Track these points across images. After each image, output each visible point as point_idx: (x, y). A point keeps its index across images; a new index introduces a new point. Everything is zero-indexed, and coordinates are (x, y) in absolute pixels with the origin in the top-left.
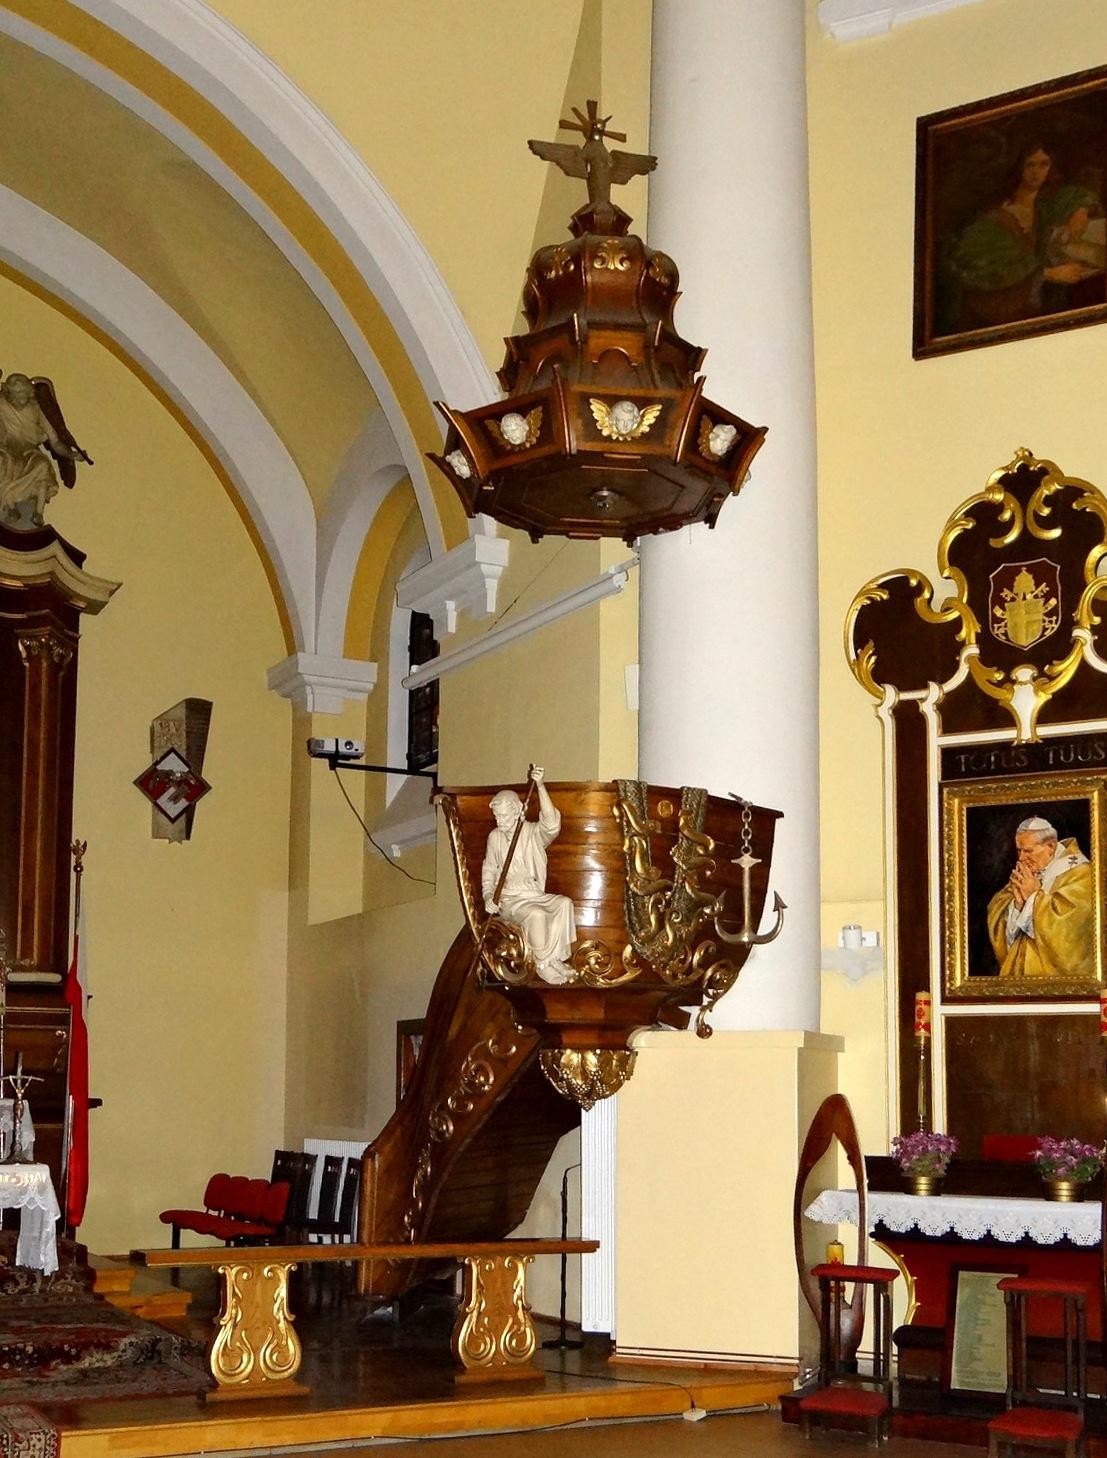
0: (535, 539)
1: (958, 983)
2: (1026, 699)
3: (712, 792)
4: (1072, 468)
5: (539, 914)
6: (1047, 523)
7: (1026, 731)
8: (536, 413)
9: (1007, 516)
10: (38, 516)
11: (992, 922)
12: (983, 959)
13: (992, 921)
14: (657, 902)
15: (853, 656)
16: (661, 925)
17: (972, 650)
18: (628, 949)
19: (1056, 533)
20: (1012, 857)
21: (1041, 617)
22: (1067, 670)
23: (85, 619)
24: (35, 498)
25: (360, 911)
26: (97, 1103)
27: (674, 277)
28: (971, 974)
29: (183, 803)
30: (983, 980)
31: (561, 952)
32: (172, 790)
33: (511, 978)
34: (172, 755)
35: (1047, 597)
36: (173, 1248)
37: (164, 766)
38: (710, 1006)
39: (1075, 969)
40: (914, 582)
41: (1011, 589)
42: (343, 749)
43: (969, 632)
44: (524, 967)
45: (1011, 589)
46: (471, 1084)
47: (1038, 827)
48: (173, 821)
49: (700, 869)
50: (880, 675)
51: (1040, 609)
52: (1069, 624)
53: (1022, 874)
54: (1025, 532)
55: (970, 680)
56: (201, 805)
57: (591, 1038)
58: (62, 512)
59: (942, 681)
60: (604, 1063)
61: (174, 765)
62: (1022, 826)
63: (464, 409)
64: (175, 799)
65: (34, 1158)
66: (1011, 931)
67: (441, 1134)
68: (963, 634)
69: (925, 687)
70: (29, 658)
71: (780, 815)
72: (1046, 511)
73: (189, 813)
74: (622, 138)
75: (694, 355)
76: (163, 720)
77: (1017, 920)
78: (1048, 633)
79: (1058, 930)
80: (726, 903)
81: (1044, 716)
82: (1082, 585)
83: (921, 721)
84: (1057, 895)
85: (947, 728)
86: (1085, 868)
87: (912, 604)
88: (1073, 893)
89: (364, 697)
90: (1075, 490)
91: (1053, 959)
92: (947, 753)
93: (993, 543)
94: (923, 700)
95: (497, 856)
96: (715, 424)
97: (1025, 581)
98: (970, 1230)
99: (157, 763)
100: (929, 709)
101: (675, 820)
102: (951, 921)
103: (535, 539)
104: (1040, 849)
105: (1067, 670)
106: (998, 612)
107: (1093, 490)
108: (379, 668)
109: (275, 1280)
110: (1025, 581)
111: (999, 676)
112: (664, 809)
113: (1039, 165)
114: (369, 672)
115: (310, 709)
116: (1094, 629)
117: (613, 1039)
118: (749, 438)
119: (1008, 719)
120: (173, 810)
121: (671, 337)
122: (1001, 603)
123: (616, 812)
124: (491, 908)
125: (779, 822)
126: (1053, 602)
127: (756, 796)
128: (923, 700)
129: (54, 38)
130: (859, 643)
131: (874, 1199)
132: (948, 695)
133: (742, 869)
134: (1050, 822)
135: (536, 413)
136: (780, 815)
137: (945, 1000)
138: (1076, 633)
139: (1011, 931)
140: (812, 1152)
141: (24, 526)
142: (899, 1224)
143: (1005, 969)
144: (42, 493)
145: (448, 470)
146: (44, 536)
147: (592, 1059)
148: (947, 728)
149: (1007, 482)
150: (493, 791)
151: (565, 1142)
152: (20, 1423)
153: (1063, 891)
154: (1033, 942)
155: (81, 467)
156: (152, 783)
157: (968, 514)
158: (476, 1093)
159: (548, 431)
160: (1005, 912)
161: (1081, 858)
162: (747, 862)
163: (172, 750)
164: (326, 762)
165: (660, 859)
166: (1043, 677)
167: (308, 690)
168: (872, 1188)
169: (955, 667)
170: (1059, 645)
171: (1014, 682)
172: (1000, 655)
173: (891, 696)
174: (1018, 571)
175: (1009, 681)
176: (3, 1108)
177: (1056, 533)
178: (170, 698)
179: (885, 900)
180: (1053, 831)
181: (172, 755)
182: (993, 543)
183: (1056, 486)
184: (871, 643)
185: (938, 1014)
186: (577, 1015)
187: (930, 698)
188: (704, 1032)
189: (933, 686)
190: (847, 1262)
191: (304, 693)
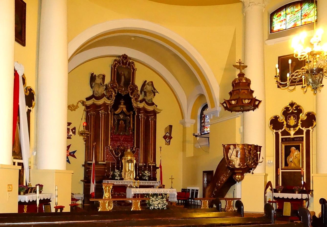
0: (231, 112)
1: (283, 167)
2: (292, 132)
3: (255, 145)
4: (298, 103)
5: (236, 160)
6: (295, 110)
7: (292, 136)
8: (236, 101)
9: (290, 109)
10: (152, 101)
11: (287, 160)
12: (286, 164)
13: (287, 160)
14: (249, 158)
15: (270, 126)
16: (249, 161)
17: (285, 126)
18: (245, 164)
19: (296, 111)
20: (290, 152)
21: (294, 122)
22: (297, 129)
25: (193, 156)
27: (250, 82)
28: (285, 166)
29: (169, 140)
30: (286, 167)
31: (238, 164)
33: (232, 167)
34: (168, 133)
35: (295, 119)
36: (203, 197)
38: (253, 170)
39: (298, 166)
40: (278, 117)
41: (290, 118)
42: (198, 135)
43: (285, 123)
44: (234, 166)
45: (290, 118)
46: (222, 179)
47: (294, 148)
48: (168, 142)
49: (254, 154)
50: (273, 128)
51: (294, 121)
52: (298, 123)
53: (291, 154)
54: (292, 111)
55: (285, 129)
56: (171, 140)
57: (240, 174)
59: (281, 129)
60: (241, 177)
61: (168, 134)
62: (291, 148)
63: (227, 100)
64: (168, 139)
66: (290, 161)
67: (218, 186)
68: (284, 123)
69: (279, 130)
70: (151, 121)
72: (295, 108)
73: (170, 141)
74: (243, 64)
75: (252, 92)
77: (291, 160)
78: (295, 124)
79: (296, 161)
81: (294, 134)
82: (299, 118)
83: (279, 134)
84: (296, 157)
85: (282, 135)
86: (299, 153)
87: (278, 120)
88: (298, 156)
89: (193, 124)
90: (298, 106)
91: (295, 164)
93: (288, 112)
94: (279, 132)
95: (230, 153)
97: (292, 117)
98: (285, 197)
99: (166, 134)
101: (251, 148)
102: (282, 160)
103: (231, 112)
104: (294, 151)
105: (297, 129)
106: (289, 121)
107: (301, 106)
108: (196, 120)
109: (207, 201)
110: (292, 117)
111: (289, 129)
112: (250, 147)
114: (194, 121)
115: (186, 126)
116: (301, 124)
117: (242, 174)
118: (260, 102)
119: (290, 135)
120: (168, 141)
121: (251, 90)
122: (289, 120)
123: (244, 147)
124: (229, 159)
125: (261, 148)
126: (296, 120)
127: (259, 145)
128: (279, 132)
129: (186, 62)
130: (271, 124)
131: (274, 193)
132: (282, 131)
133: (258, 154)
134: (295, 147)
135: (236, 101)
137: (281, 170)
138: (298, 124)
139: (290, 161)
140: (267, 187)
141: (150, 102)
142: (277, 196)
143: (289, 166)
145: (223, 106)
146: (153, 104)
147: (240, 176)
148: (282, 135)
149: (290, 105)
150: (230, 145)
151: (232, 187)
153: (296, 156)
154: (293, 162)
155: (156, 93)
156: (165, 137)
157: (285, 108)
158: (223, 180)
160: (289, 159)
161: (299, 152)
162: (259, 153)
163: (168, 132)
164: (195, 136)
165: (249, 153)
166: (294, 129)
167: (186, 124)
168: (274, 192)
169: (283, 128)
170: (296, 126)
171: (291, 130)
172: (289, 126)
173: (275, 131)
174: (291, 116)
175: (290, 130)
177: (296, 111)
178: (167, 125)
179: (273, 157)
180: (295, 149)
181: (168, 133)
182: (288, 112)
183: (296, 105)
184: (272, 124)
185: (280, 171)
186: (238, 172)
188: (253, 173)
189: (280, 130)
190: (271, 201)
191: (185, 124)
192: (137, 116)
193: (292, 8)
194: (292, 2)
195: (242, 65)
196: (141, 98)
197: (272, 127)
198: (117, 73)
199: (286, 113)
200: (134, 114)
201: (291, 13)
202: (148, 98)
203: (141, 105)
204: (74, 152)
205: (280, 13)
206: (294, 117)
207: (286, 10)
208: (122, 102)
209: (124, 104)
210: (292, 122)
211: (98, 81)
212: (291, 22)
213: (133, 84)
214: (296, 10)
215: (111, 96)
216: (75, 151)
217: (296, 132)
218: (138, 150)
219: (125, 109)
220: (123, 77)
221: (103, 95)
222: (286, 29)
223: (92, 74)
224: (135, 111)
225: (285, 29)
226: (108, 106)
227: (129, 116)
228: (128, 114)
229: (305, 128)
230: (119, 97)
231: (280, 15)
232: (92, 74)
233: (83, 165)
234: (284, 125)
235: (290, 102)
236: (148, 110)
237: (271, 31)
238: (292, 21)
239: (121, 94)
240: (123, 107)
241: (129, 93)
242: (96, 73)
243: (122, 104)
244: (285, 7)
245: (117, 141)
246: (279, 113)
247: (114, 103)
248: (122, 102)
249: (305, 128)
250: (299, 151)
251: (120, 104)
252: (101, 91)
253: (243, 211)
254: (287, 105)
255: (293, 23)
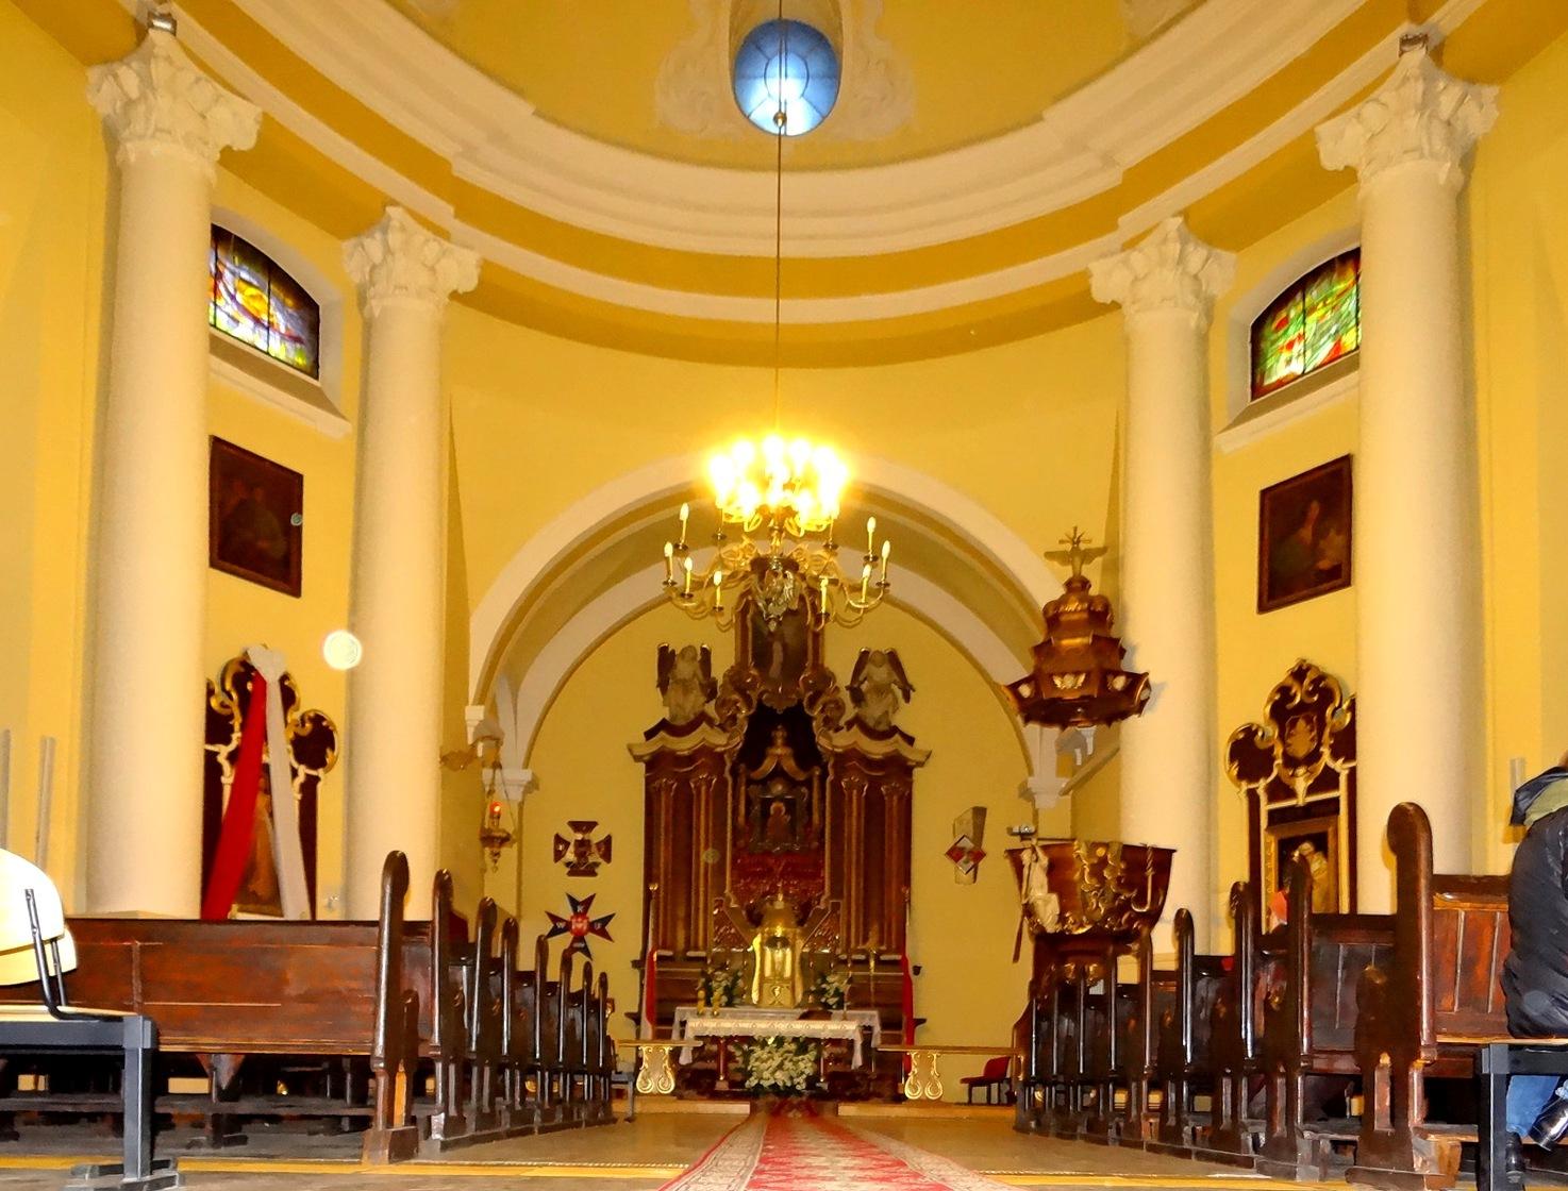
2: (1301, 784)
7: (1301, 799)
9: (1293, 691)
17: (1279, 761)
22: (1320, 767)
23: (917, 772)
24: (887, 712)
26: (923, 1021)
29: (972, 863)
32: (965, 858)
37: (960, 845)
43: (1279, 751)
50: (1241, 776)
55: (1277, 777)
56: (981, 864)
58: (904, 719)
61: (967, 844)
65: (1008, 1101)
71: (1174, 851)
73: (975, 867)
74: (1090, 541)
76: (960, 820)
80: (1138, 893)
81: (1311, 790)
85: (1271, 800)
90: (1322, 677)
92: (129, 949)
96: (1115, 677)
97: (1301, 724)
100: (1261, 792)
105: (1320, 767)
110: (1301, 724)
113: (1315, 508)
116: (1331, 746)
125: (1174, 854)
135: (1033, 682)
136: (1174, 851)
141: (882, 727)
144: (890, 710)
146: (894, 730)
148: (1271, 800)
152: (697, 1024)
155: (912, 694)
159: (1037, 691)
169: (1272, 771)
173: (1245, 786)
176: (294, 798)
187: (1261, 786)
192: (832, 782)
193: (1325, 284)
194: (1325, 261)
195: (1083, 546)
196: (850, 711)
197: (1235, 772)
198: (754, 633)
199: (1282, 709)
200: (824, 775)
201: (1321, 305)
202: (873, 711)
203: (842, 740)
204: (606, 920)
205: (1283, 314)
206: (1309, 721)
207: (1304, 299)
208: (780, 735)
209: (787, 743)
210: (1301, 744)
211: (685, 669)
212: (1323, 340)
213: (818, 666)
214: (1340, 287)
215: (734, 718)
216: (610, 917)
217: (1316, 780)
218: (836, 907)
219: (789, 765)
220: (777, 647)
221: (702, 718)
222: (1303, 374)
223: (663, 651)
224: (827, 763)
225: (1299, 372)
226: (721, 755)
227: (808, 783)
228: (801, 777)
229: (1344, 762)
230: (762, 725)
231: (1285, 321)
232: (666, 648)
233: (636, 964)
234: (1273, 759)
235: (1292, 664)
236: (678, 753)
237: (1257, 389)
238: (1326, 338)
239: (772, 710)
240: (779, 753)
241: (800, 702)
242: (676, 646)
243: (779, 741)
244: (1302, 285)
245: (762, 875)
246: (1255, 710)
247: (743, 745)
248: (780, 735)
249: (1344, 762)
250: (1326, 855)
251: (771, 743)
252: (694, 702)
253: (1114, 1103)
254: (1280, 676)
255: (1330, 345)
